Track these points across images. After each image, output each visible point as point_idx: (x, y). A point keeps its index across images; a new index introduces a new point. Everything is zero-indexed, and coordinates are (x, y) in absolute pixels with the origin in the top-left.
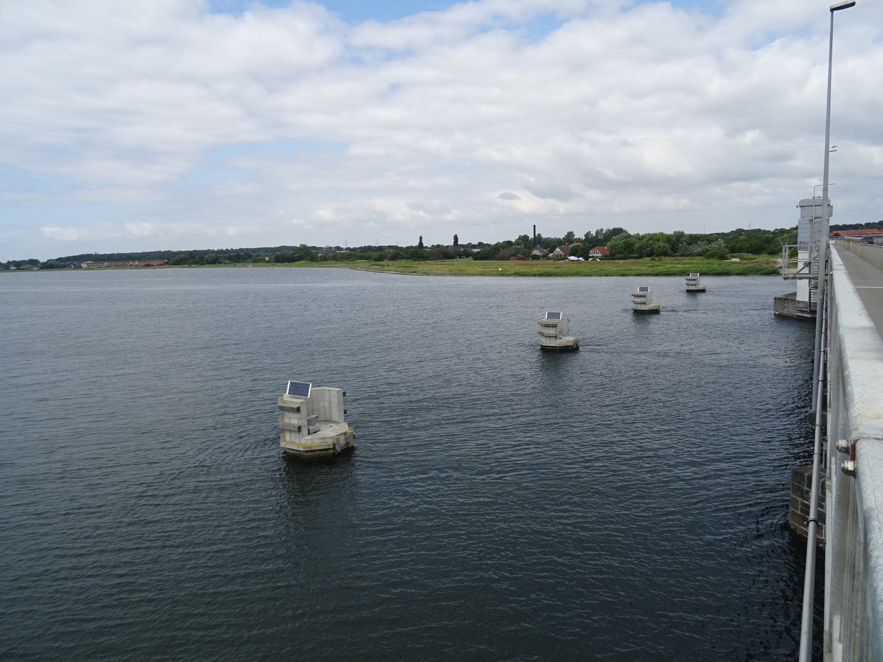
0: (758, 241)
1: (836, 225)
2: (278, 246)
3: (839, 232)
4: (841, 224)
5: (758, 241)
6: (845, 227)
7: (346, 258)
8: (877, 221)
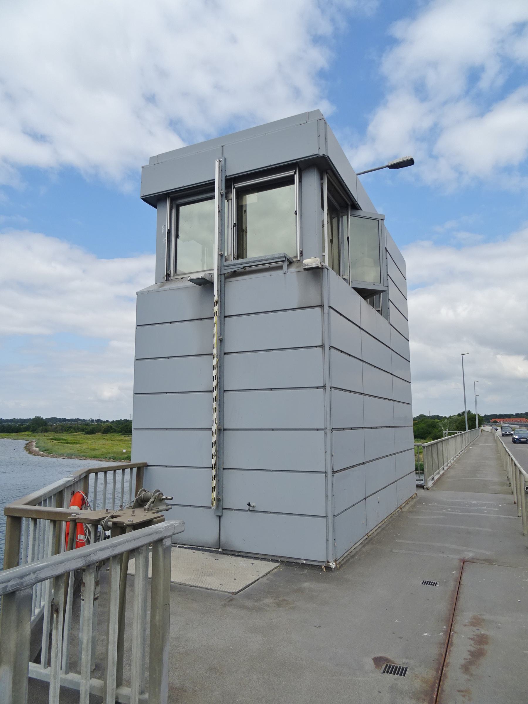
0: (424, 425)
1: (495, 415)
2: (10, 418)
3: (497, 420)
4: (498, 414)
5: (424, 425)
6: (501, 416)
7: (65, 431)
8: (524, 413)
